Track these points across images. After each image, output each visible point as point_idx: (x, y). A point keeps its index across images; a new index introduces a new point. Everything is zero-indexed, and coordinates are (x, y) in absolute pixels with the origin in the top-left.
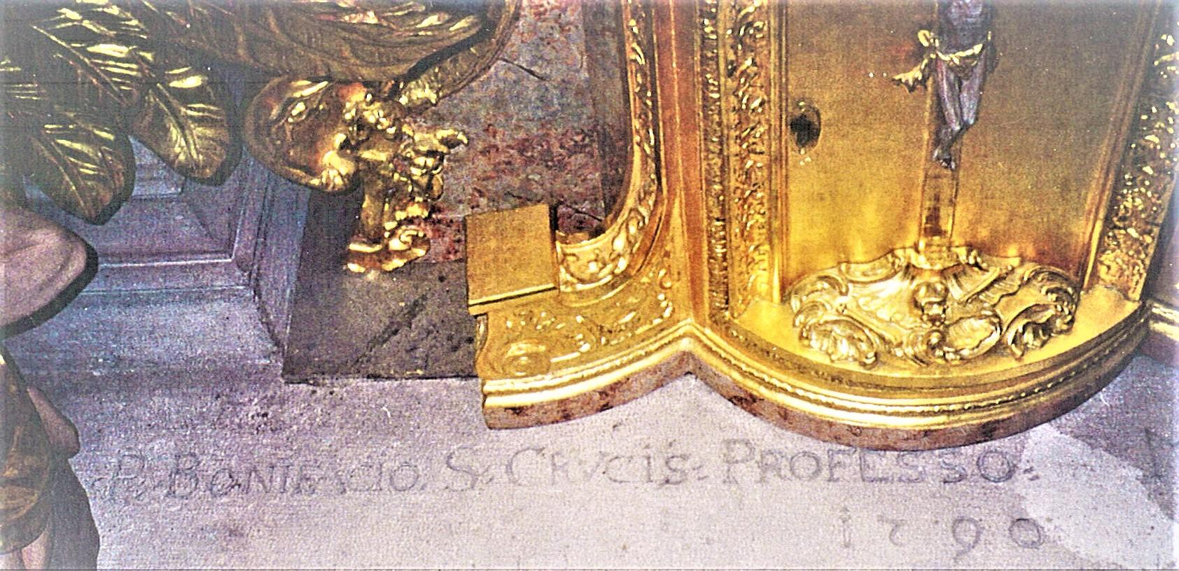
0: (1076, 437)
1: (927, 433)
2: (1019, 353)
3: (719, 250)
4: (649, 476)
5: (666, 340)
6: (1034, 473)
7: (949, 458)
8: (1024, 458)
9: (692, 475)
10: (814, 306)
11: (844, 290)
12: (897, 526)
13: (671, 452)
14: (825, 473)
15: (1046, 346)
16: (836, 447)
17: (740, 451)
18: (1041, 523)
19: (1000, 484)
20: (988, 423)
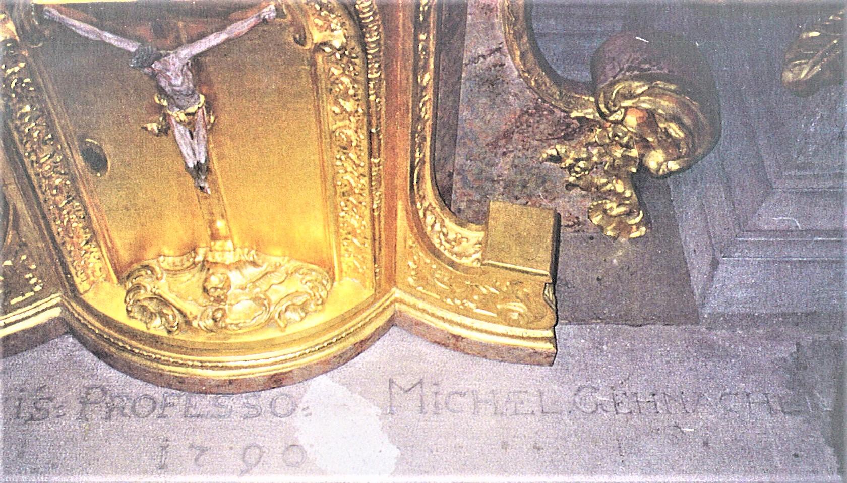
0: (343, 384)
1: (231, 382)
2: (282, 325)
3: (344, 335)
4: (422, 407)
5: (40, 309)
6: (305, 413)
7: (252, 401)
8: (304, 399)
9: (54, 413)
10: (138, 287)
11: (159, 276)
12: (203, 450)
13: (40, 395)
14: (158, 411)
15: (304, 321)
16: (170, 391)
17: (96, 394)
18: (306, 447)
19: (283, 419)
20: (275, 375)
